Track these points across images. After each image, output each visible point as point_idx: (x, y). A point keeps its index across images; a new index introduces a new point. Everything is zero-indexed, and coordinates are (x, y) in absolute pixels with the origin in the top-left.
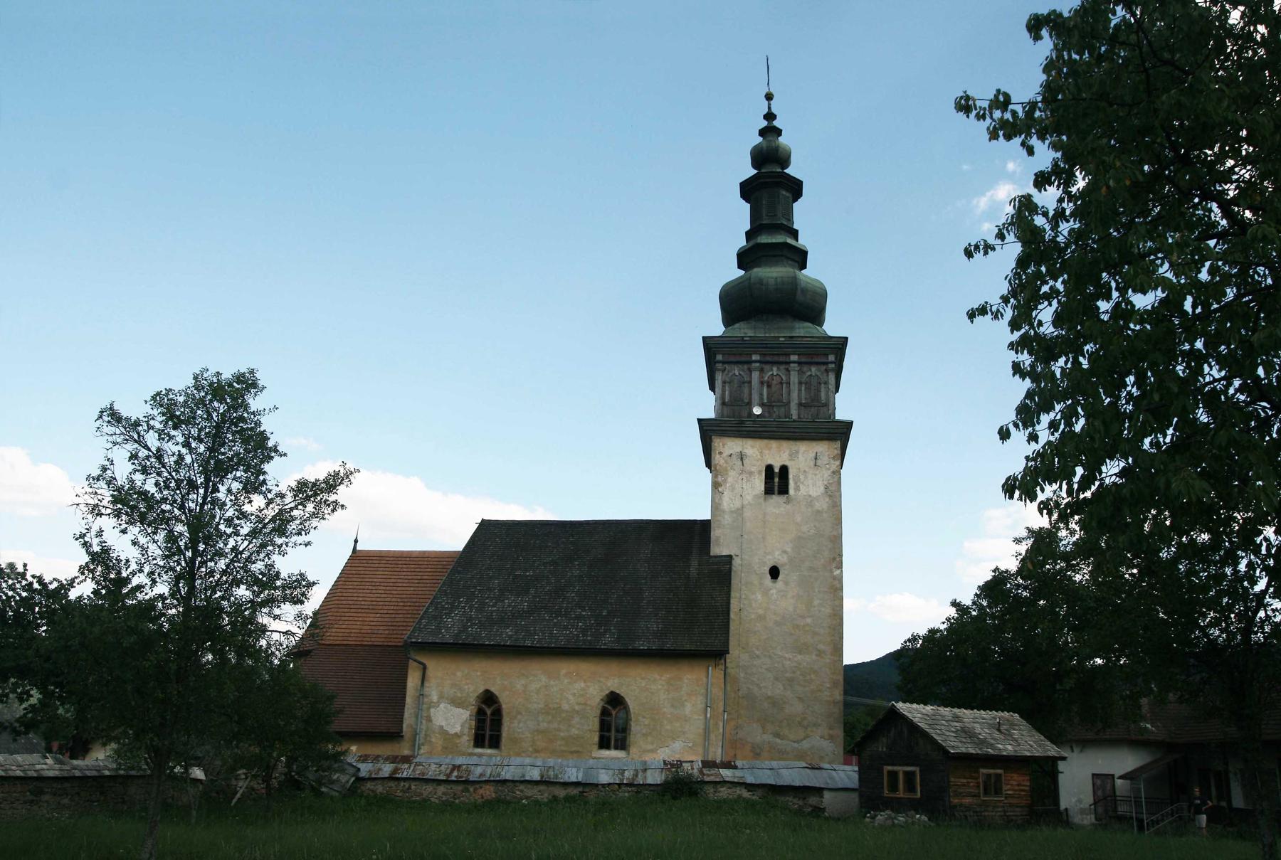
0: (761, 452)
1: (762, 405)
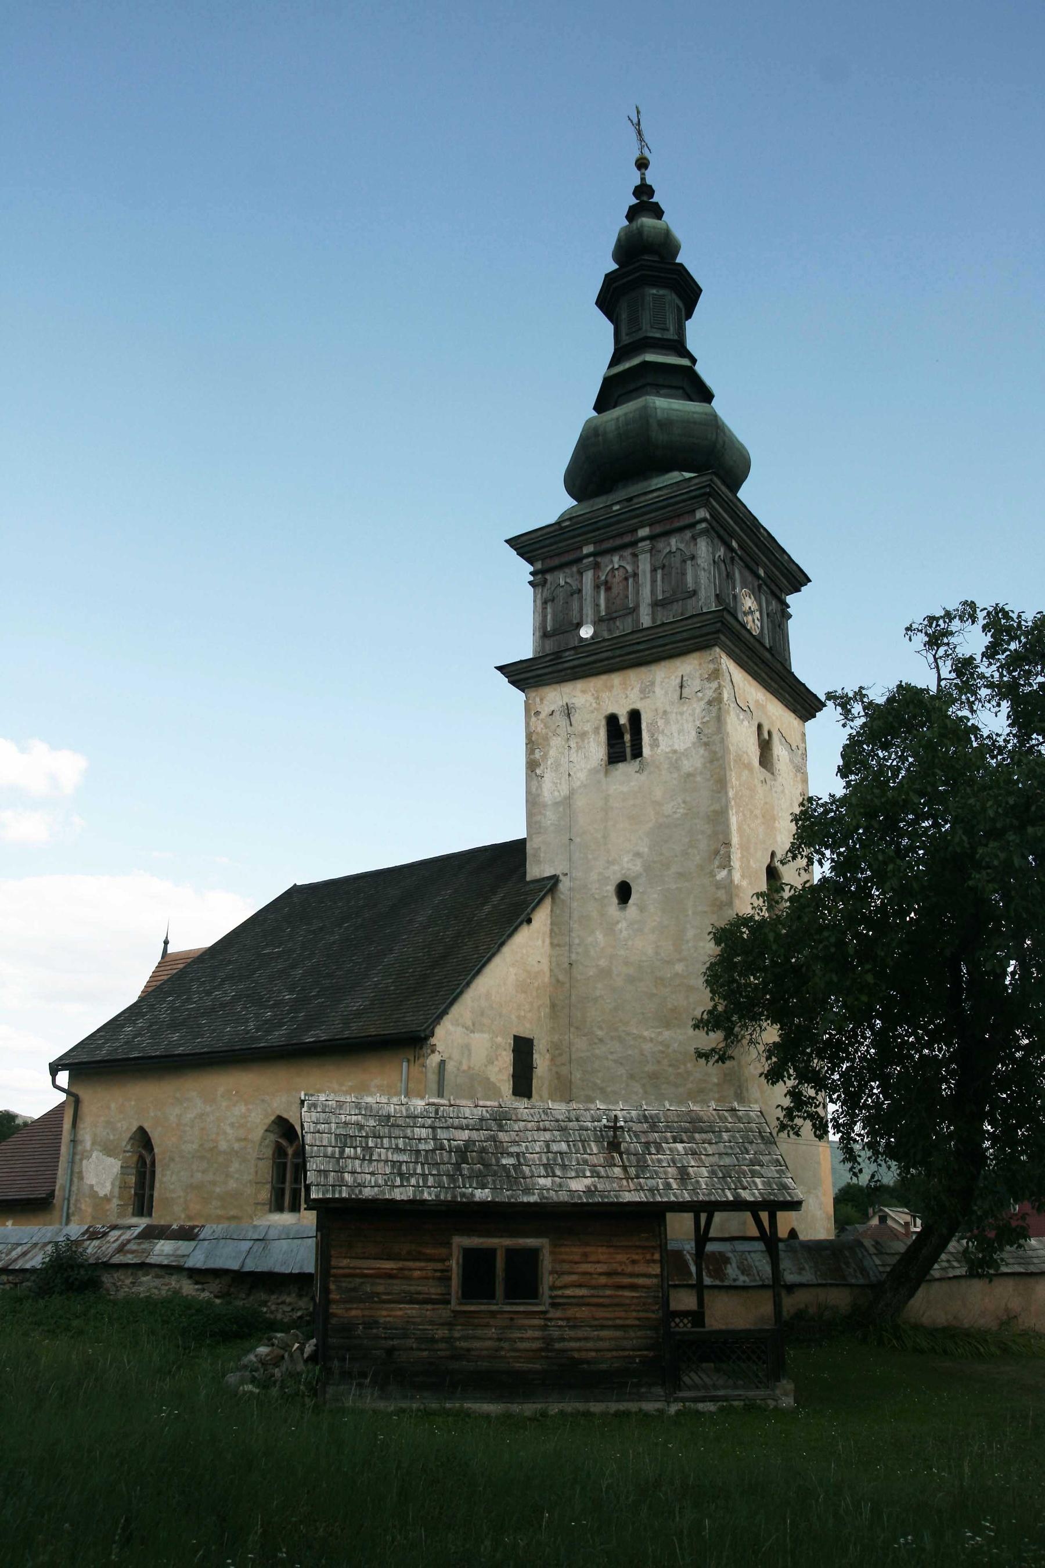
0: (597, 698)
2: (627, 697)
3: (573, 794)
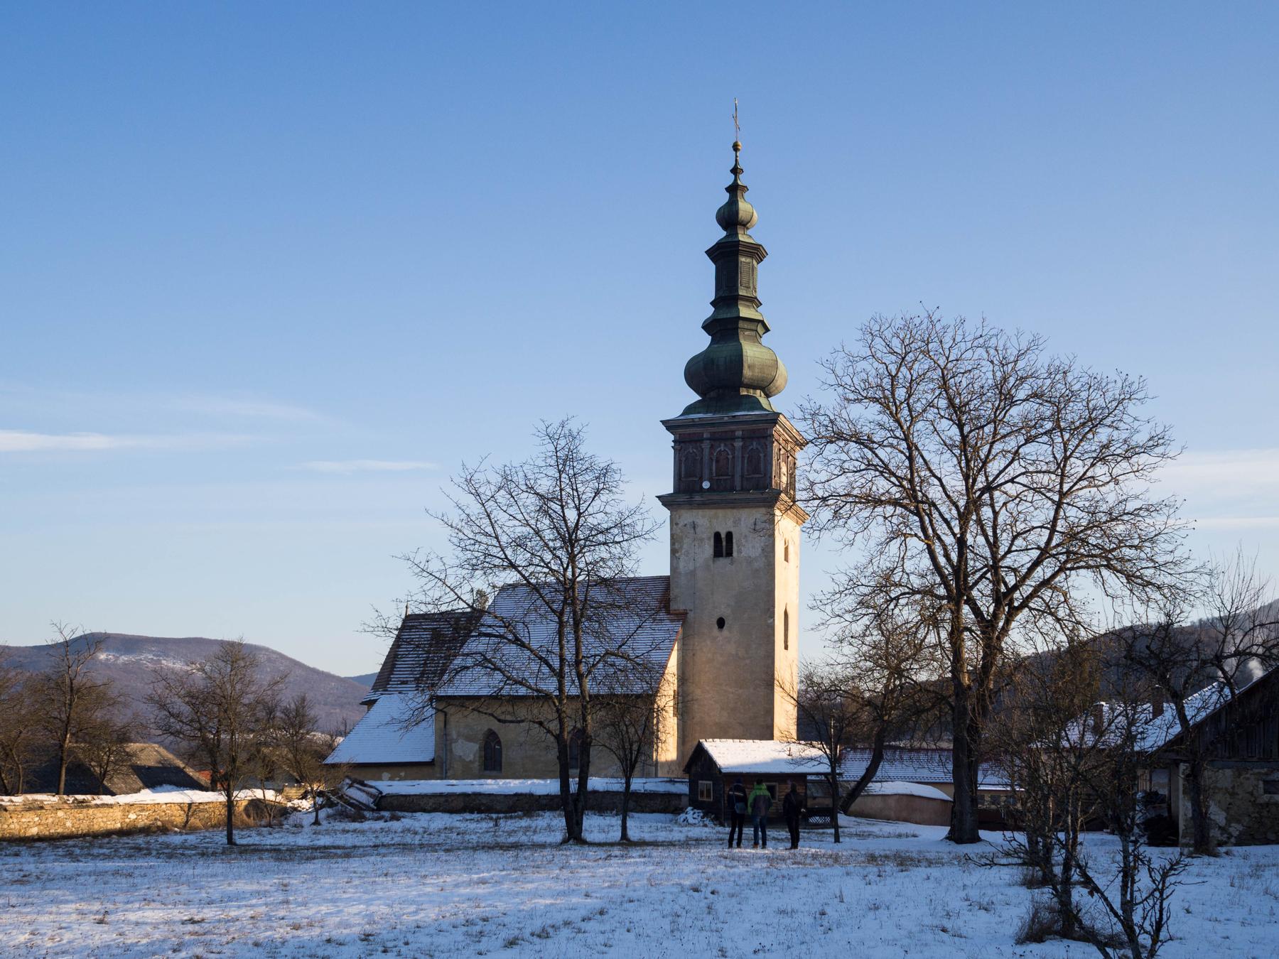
1: (710, 480)
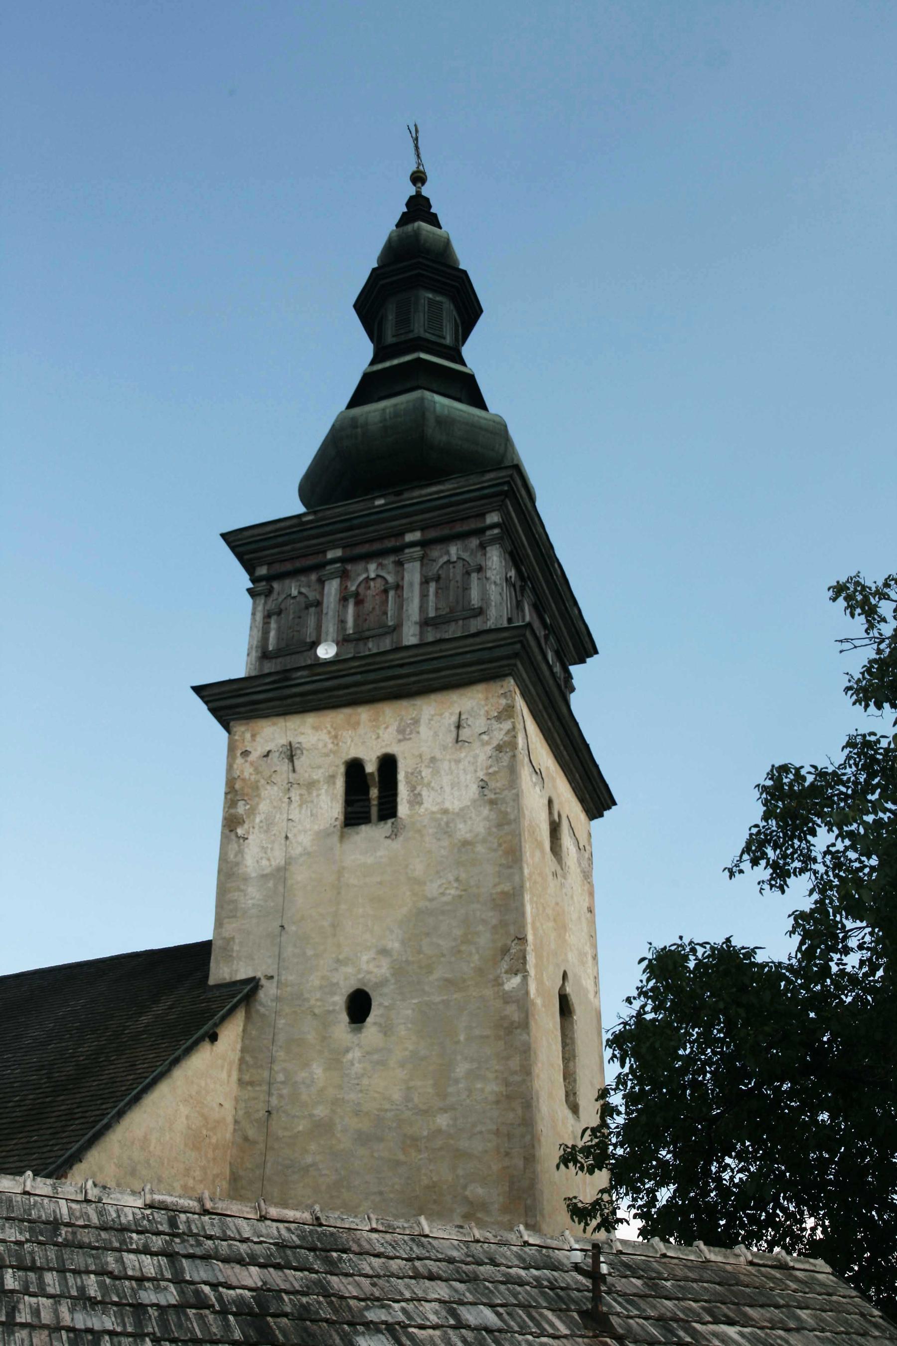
2: (378, 737)
3: (290, 864)
